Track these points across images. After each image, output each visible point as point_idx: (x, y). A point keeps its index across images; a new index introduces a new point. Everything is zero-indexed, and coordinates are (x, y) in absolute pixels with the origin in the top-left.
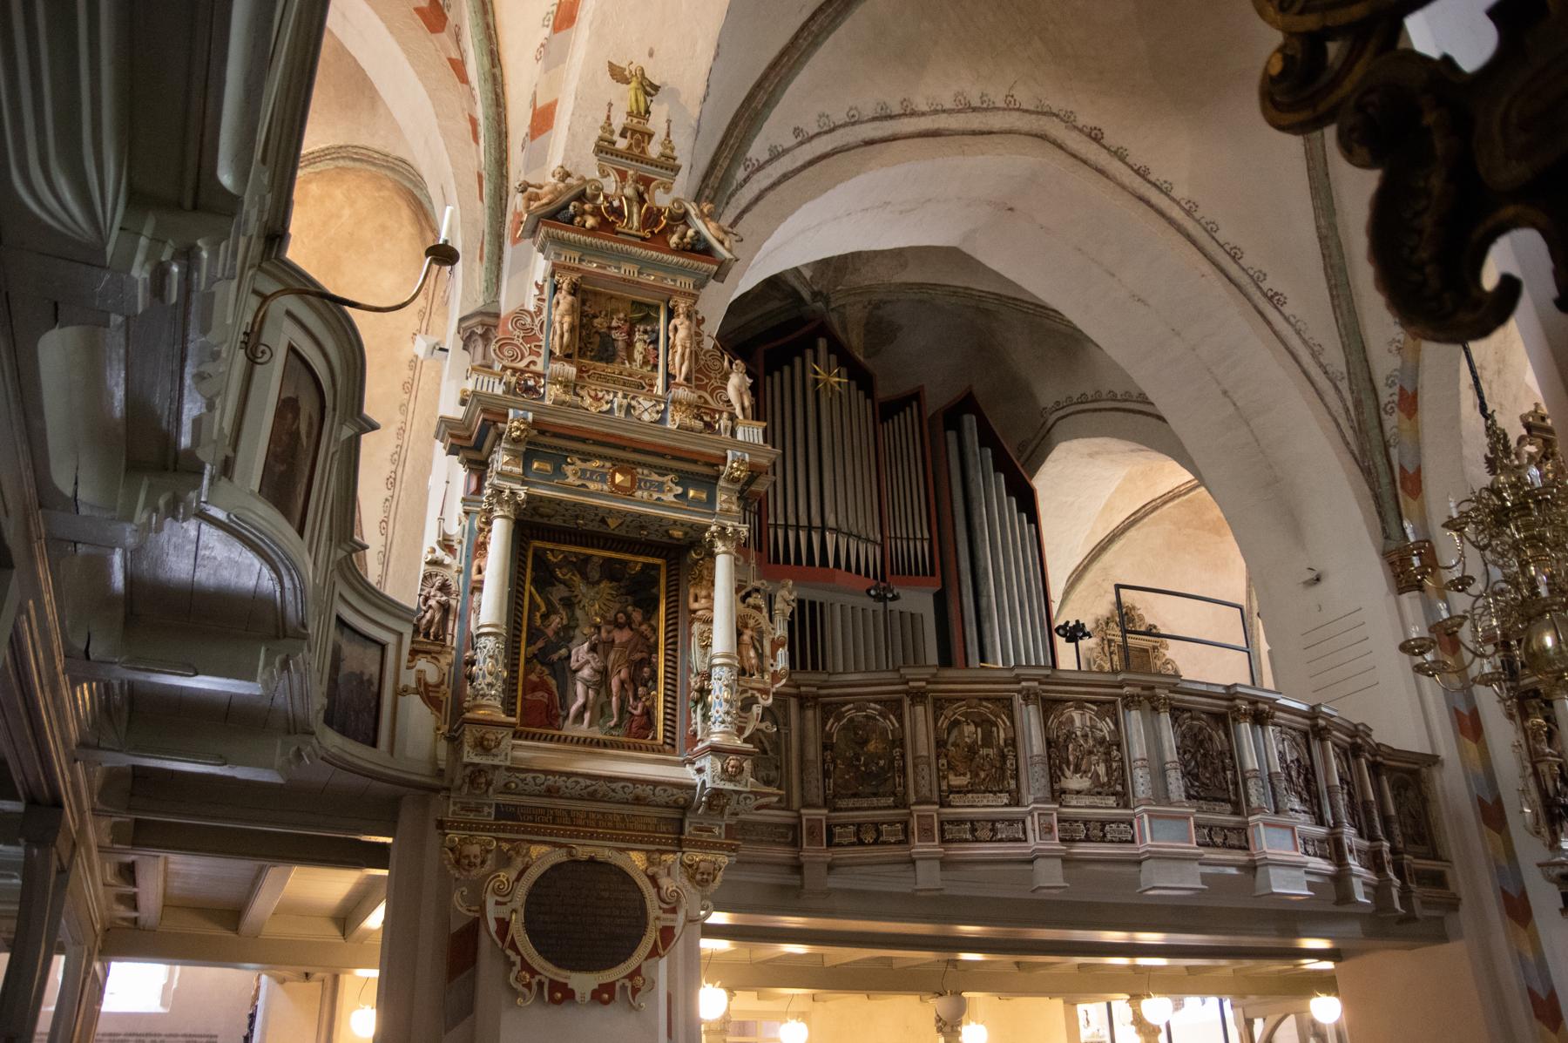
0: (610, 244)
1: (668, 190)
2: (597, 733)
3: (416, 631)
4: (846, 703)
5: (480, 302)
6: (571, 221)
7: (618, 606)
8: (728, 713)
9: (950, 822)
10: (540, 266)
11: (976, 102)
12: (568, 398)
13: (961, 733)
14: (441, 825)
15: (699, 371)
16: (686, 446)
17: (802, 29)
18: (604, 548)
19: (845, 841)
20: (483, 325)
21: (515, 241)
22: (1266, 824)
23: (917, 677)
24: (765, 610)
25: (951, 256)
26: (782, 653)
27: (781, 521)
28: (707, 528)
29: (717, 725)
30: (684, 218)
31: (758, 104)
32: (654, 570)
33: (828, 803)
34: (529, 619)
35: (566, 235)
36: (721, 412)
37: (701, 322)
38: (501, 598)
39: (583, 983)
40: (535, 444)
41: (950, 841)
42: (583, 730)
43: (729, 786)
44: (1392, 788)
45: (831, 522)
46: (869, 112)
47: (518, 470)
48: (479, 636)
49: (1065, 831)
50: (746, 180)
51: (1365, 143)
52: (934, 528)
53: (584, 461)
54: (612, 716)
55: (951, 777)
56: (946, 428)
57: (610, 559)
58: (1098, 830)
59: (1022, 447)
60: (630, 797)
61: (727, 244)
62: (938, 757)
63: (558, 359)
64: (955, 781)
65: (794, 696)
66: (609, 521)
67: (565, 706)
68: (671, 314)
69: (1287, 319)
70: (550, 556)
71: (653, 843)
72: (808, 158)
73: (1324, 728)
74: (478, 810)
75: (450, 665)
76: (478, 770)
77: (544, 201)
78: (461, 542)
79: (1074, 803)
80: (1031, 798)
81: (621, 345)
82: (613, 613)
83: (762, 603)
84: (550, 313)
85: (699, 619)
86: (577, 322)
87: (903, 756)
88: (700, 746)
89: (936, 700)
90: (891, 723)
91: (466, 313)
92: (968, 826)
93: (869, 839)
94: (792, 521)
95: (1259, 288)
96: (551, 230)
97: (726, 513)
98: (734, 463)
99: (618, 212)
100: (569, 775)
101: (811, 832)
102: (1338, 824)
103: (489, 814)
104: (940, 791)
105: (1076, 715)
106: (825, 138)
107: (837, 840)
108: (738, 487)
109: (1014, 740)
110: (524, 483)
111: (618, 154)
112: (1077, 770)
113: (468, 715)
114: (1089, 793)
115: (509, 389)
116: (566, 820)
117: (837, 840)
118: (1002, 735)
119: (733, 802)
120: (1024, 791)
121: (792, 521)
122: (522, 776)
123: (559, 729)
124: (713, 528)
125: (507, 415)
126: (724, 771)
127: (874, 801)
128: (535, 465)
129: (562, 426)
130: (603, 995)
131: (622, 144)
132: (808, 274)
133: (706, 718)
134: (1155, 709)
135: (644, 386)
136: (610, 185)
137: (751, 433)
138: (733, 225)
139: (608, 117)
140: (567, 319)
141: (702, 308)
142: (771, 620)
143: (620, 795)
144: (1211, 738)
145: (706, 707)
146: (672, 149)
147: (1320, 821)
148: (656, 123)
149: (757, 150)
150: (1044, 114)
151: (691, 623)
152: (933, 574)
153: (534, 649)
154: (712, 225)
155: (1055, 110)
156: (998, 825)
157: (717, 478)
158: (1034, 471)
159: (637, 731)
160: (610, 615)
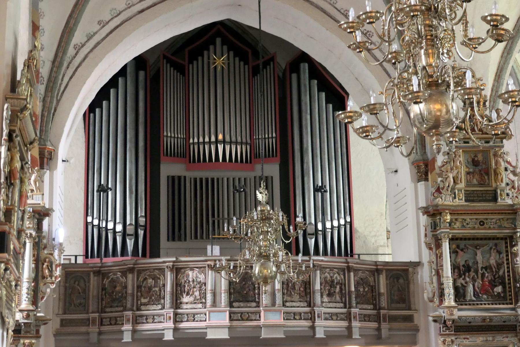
8: (27, 297)
13: (147, 283)
56: (291, 72)
58: (193, 317)
62: (137, 292)
64: (143, 301)
90: (123, 280)
105: (190, 273)
112: (188, 294)
114: (191, 303)
118: (161, 283)
126: (23, 317)
127: (398, 305)
149: (71, 51)
152: (276, 156)
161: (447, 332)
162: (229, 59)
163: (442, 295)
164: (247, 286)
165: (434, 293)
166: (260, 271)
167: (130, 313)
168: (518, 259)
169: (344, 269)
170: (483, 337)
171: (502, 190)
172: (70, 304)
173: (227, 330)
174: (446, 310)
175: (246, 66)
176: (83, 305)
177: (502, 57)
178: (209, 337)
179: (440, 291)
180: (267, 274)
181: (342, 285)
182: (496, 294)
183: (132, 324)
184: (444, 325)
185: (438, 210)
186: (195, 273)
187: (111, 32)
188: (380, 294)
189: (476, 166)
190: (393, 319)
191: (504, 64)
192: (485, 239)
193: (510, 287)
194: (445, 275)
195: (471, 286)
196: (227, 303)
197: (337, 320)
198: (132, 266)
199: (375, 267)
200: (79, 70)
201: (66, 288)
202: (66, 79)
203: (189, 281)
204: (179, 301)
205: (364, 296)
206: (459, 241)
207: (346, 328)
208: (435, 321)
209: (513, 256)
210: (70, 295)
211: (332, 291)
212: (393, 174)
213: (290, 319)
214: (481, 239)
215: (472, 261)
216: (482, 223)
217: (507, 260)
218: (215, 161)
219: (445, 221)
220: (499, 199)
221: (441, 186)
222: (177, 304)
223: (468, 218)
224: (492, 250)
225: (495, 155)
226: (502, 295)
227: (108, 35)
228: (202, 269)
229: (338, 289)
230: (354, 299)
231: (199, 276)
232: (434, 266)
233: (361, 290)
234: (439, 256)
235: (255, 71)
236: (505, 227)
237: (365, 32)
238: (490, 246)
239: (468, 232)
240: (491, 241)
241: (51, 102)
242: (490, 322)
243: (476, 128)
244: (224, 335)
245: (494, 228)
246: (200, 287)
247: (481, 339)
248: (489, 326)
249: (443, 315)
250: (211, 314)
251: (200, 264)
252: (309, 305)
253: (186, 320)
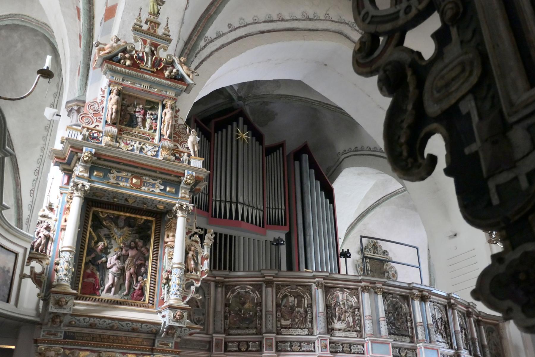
0: (136, 73)
1: (165, 49)
2: (117, 298)
3: (32, 248)
4: (236, 285)
5: (77, 95)
6: (119, 61)
7: (131, 239)
8: (178, 290)
9: (281, 342)
10: (105, 81)
11: (311, 17)
12: (112, 143)
13: (288, 301)
14: (36, 341)
15: (175, 133)
16: (166, 168)
18: (126, 212)
19: (233, 349)
20: (77, 105)
21: (94, 68)
22: (425, 348)
23: (269, 275)
24: (200, 243)
25: (299, 84)
26: (206, 263)
27: (218, 199)
28: (174, 205)
29: (173, 297)
30: (172, 64)
31: (211, 12)
32: (147, 225)
33: (226, 332)
34: (89, 244)
35: (117, 68)
36: (184, 153)
37: (177, 111)
38: (75, 234)
40: (95, 163)
41: (281, 351)
42: (111, 296)
43: (176, 324)
44: (486, 332)
45: (241, 200)
46: (262, 18)
47: (87, 175)
48: (62, 251)
49: (333, 348)
50: (205, 47)
51: (388, 85)
52: (287, 205)
54: (125, 290)
55: (282, 321)
56: (295, 160)
57: (130, 217)
59: (328, 170)
60: (130, 329)
61: (191, 76)
63: (109, 125)
64: (284, 323)
65: (214, 281)
66: (129, 200)
67: (102, 284)
68: (164, 107)
70: (101, 215)
71: (139, 350)
72: (234, 38)
73: (454, 304)
74: (55, 335)
75: (48, 264)
76: (57, 315)
77: (107, 51)
78: (57, 207)
79: (337, 335)
80: (318, 332)
81: (139, 120)
82: (129, 242)
83: (199, 240)
84: (107, 104)
85: (168, 246)
86: (119, 109)
87: (261, 311)
88: (165, 304)
89: (277, 285)
90: (255, 295)
91: (69, 99)
92: (289, 344)
93: (243, 349)
94: (223, 199)
96: (109, 65)
97: (183, 198)
98: (188, 176)
99: (141, 59)
100: (101, 318)
101: (217, 345)
102: (459, 348)
103: (61, 336)
104: (277, 327)
105: (340, 294)
106: (242, 29)
107: (229, 349)
108: (189, 187)
109: (311, 305)
110: (89, 181)
111: (143, 32)
112: (339, 319)
113: (53, 289)
114: (344, 330)
115: (84, 138)
116: (99, 340)
117: (229, 349)
119: (178, 332)
120: (315, 328)
121: (223, 199)
122: (78, 318)
123: (99, 296)
124: (177, 205)
125: (82, 150)
126: (174, 317)
127: (247, 331)
128: (95, 173)
129: (108, 156)
131: (145, 27)
132: (236, 88)
133: (168, 292)
134: (376, 293)
135: (148, 139)
136: (139, 46)
137: (197, 163)
138: (196, 68)
139: (140, 15)
140: (115, 107)
141: (179, 106)
142: (202, 247)
143: (126, 328)
144: (401, 307)
145: (169, 286)
146: (169, 31)
147: (451, 347)
148: (162, 19)
149: (210, 33)
150: (342, 23)
151: (165, 247)
152: (285, 225)
153: (90, 258)
154: (185, 67)
155: (346, 22)
156: (303, 344)
157: (180, 183)
158: (333, 181)
159: (136, 297)
160: (127, 243)
176: (202, 322)
186: (345, 294)
198: (271, 278)
200: (204, 63)
218: (235, 219)
231: (350, 299)
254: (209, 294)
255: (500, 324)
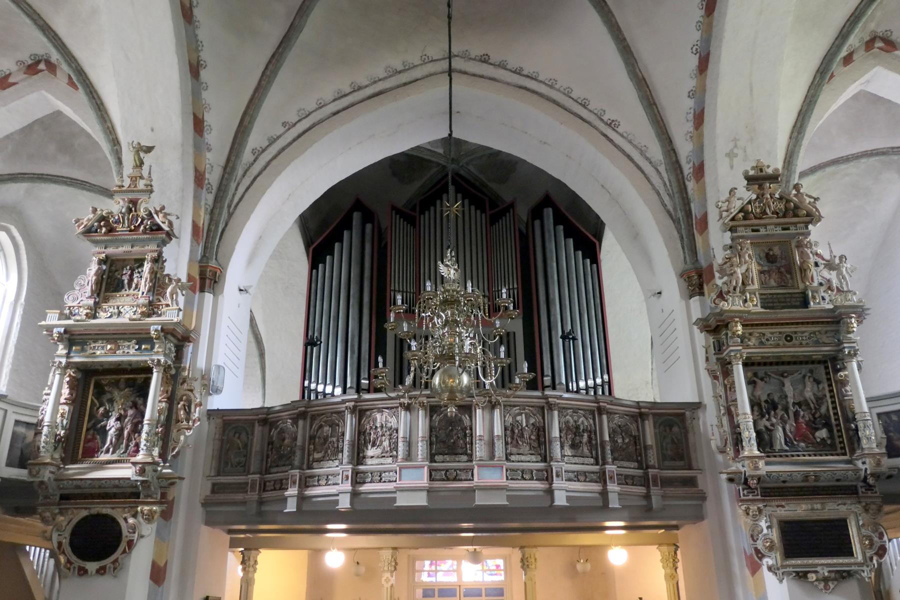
2: (115, 457)
11: (400, 67)
13: (323, 432)
17: (262, 76)
31: (246, 123)
39: (92, 566)
46: (330, 97)
53: (94, 342)
56: (533, 219)
57: (129, 379)
62: (309, 444)
64: (317, 456)
69: (622, 136)
72: (296, 135)
81: (126, 282)
95: (602, 120)
105: (378, 416)
106: (304, 121)
112: (374, 445)
114: (378, 457)
127: (673, 463)
130: (101, 571)
140: (94, 278)
146: (151, 181)
149: (247, 156)
161: (751, 497)
162: (463, 207)
163: (738, 441)
164: (455, 432)
165: (726, 440)
166: (443, 381)
167: (296, 472)
168: (848, 388)
169: (594, 411)
170: (806, 504)
171: (815, 291)
172: (226, 463)
173: (425, 494)
174: (747, 462)
175: (483, 215)
177: (790, 138)
178: (399, 503)
179: (735, 436)
180: (454, 385)
181: (591, 432)
182: (819, 440)
183: (299, 487)
184: (745, 486)
185: (723, 321)
187: (299, 136)
188: (646, 448)
189: (772, 262)
190: (667, 482)
191: (795, 146)
192: (795, 363)
193: (839, 431)
194: (740, 412)
195: (780, 429)
196: (425, 455)
197: (585, 481)
198: (303, 409)
199: (637, 410)
200: (259, 178)
201: (222, 441)
202: (241, 189)
203: (376, 427)
204: (361, 455)
205: (624, 450)
206: (756, 368)
207: (600, 493)
208: (731, 480)
209: (839, 385)
210: (228, 450)
211: (577, 441)
212: (654, 299)
213: (517, 479)
214: (789, 363)
215: (779, 395)
216: (789, 338)
217: (831, 391)
219: (734, 333)
220: (812, 303)
221: (725, 289)
222: (358, 458)
223: (767, 331)
224: (807, 378)
225: (799, 245)
226: (829, 442)
227: (294, 140)
228: (393, 410)
229: (585, 438)
230: (609, 452)
232: (722, 401)
233: (620, 441)
234: (730, 388)
235: (494, 220)
236: (824, 343)
237: (609, 122)
238: (803, 373)
239: (768, 351)
240: (804, 366)
241: (220, 214)
242: (816, 481)
243: (768, 211)
244: (420, 500)
245: (807, 345)
246: (391, 435)
247: (804, 507)
248: (815, 487)
249: (743, 470)
250: (403, 471)
251: (390, 404)
252: (544, 460)
253: (369, 480)
254: (253, 434)
255: (687, 413)
